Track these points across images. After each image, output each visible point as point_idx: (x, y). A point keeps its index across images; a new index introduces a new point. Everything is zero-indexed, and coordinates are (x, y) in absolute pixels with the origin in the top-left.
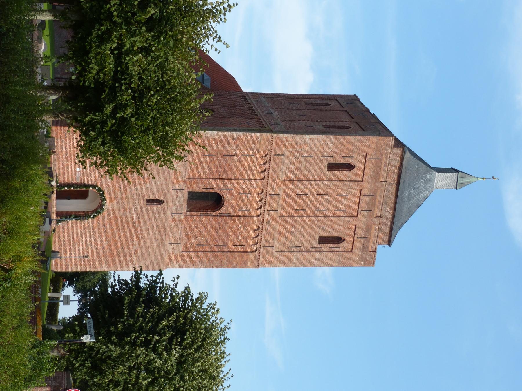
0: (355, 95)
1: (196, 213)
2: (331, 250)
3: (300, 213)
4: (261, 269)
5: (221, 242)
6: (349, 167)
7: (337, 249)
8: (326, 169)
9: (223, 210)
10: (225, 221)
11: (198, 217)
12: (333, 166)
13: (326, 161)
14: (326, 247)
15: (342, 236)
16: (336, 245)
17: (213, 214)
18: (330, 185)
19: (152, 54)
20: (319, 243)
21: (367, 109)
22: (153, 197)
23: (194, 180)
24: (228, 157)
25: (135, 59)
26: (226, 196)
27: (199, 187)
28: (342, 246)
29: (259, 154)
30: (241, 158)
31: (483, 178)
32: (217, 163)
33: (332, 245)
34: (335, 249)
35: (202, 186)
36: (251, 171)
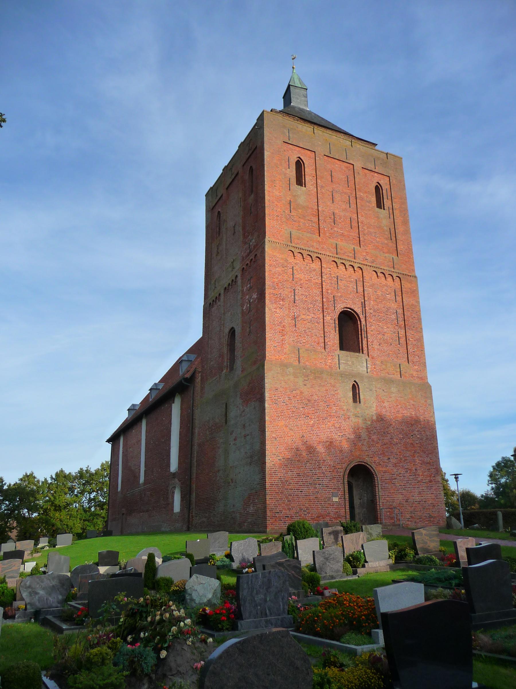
0: (207, 195)
1: (365, 342)
2: (389, 197)
3: (355, 224)
4: (417, 273)
5: (394, 317)
6: (299, 165)
7: (389, 190)
8: (303, 188)
9: (358, 310)
10: (370, 309)
11: (369, 340)
12: (300, 181)
13: (295, 187)
14: (387, 203)
15: (230, 328)
16: (384, 192)
17: (363, 320)
18: (322, 187)
19: (98, 636)
20: (384, 209)
21: (223, 170)
22: (350, 394)
23: (326, 341)
24: (297, 298)
25: (356, 608)
26: (340, 307)
27: (334, 337)
28: (385, 186)
29: (291, 260)
30: (296, 282)
31: (293, 68)
32: (304, 312)
33: (385, 197)
34: (389, 194)
35: (333, 332)
36: (310, 272)
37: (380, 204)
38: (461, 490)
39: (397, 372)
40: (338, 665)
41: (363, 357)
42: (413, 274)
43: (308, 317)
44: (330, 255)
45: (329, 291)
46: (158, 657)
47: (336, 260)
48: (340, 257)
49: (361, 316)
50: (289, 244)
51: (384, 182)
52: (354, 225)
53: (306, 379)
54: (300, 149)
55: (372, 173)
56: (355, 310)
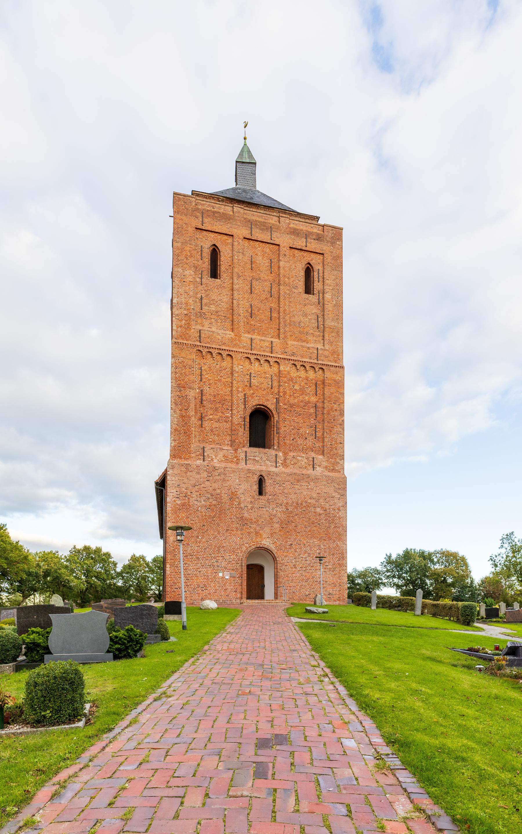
2: (321, 279)
6: (215, 253)
12: (214, 274)
13: (207, 279)
14: (317, 286)
16: (316, 274)
24: (204, 398)
26: (253, 403)
27: (244, 434)
33: (316, 279)
34: (321, 275)
37: (308, 289)
38: (402, 553)
39: (309, 465)
40: (274, 815)
41: (271, 452)
42: (339, 365)
43: (215, 417)
44: (242, 351)
45: (240, 390)
46: (203, 646)
47: (249, 356)
48: (254, 352)
49: (274, 412)
50: (198, 344)
51: (316, 261)
52: (275, 315)
53: (210, 475)
54: (216, 235)
55: (302, 253)
56: (268, 406)
